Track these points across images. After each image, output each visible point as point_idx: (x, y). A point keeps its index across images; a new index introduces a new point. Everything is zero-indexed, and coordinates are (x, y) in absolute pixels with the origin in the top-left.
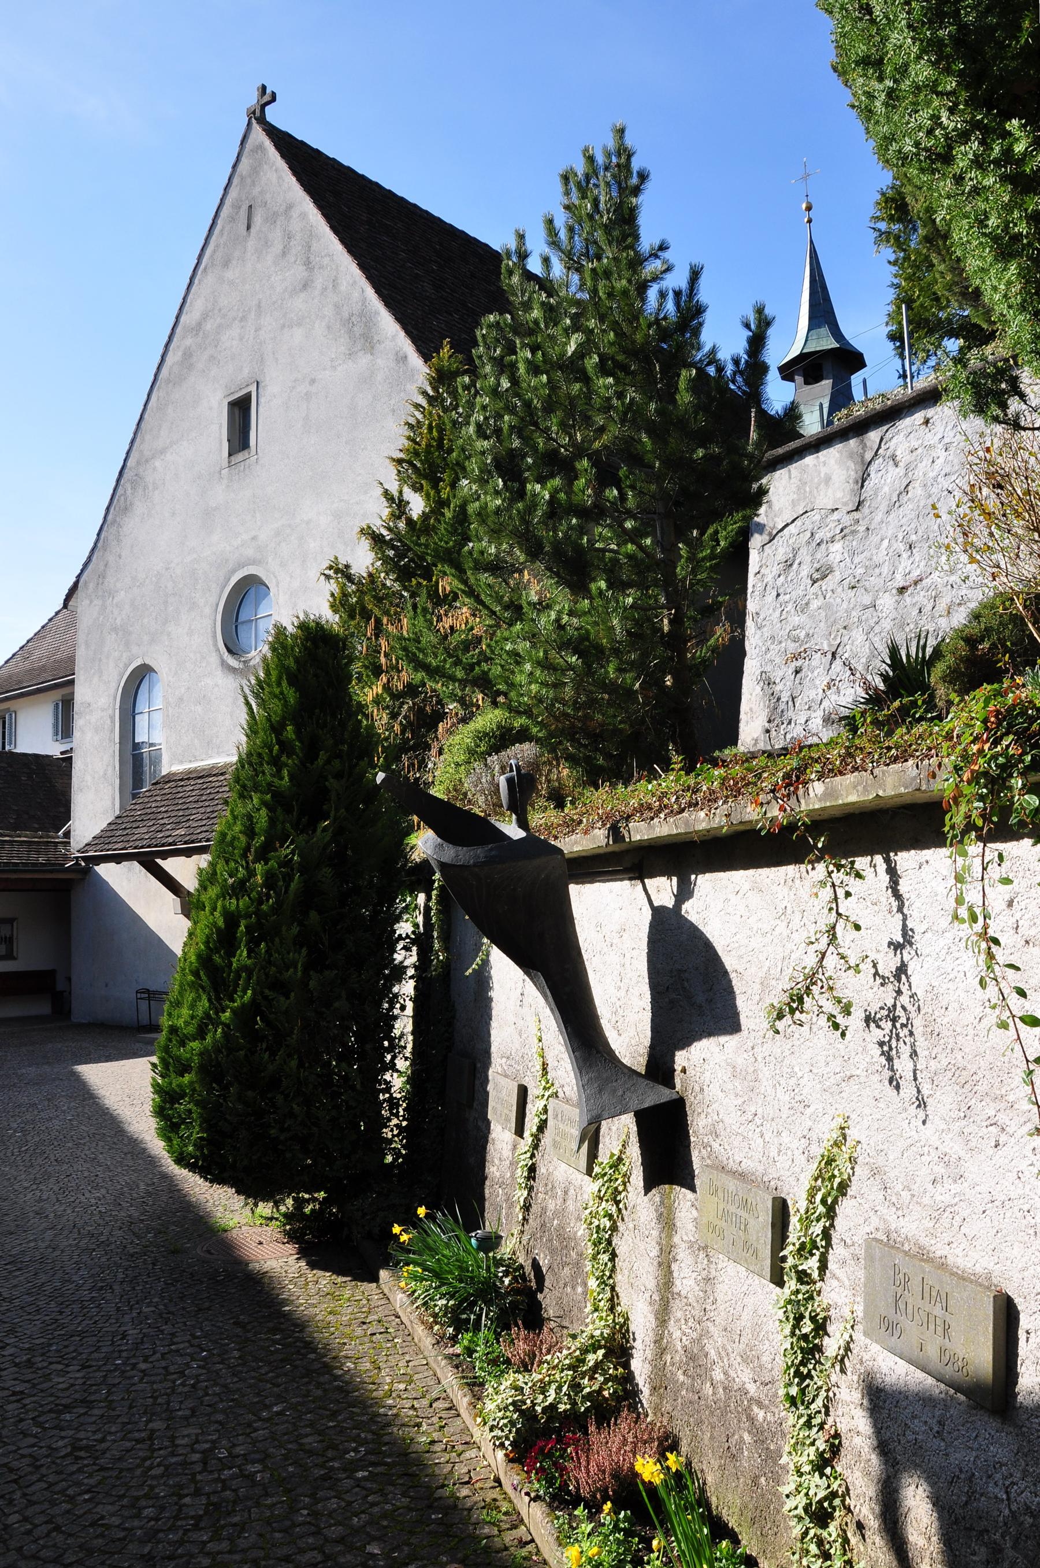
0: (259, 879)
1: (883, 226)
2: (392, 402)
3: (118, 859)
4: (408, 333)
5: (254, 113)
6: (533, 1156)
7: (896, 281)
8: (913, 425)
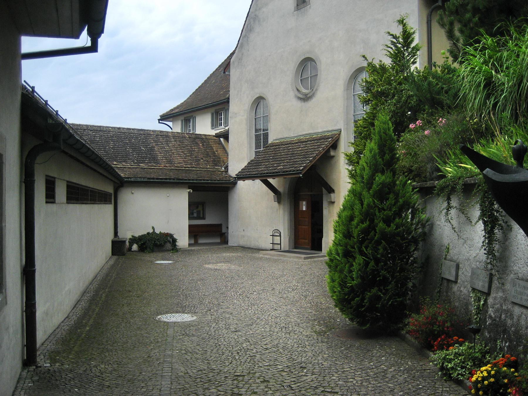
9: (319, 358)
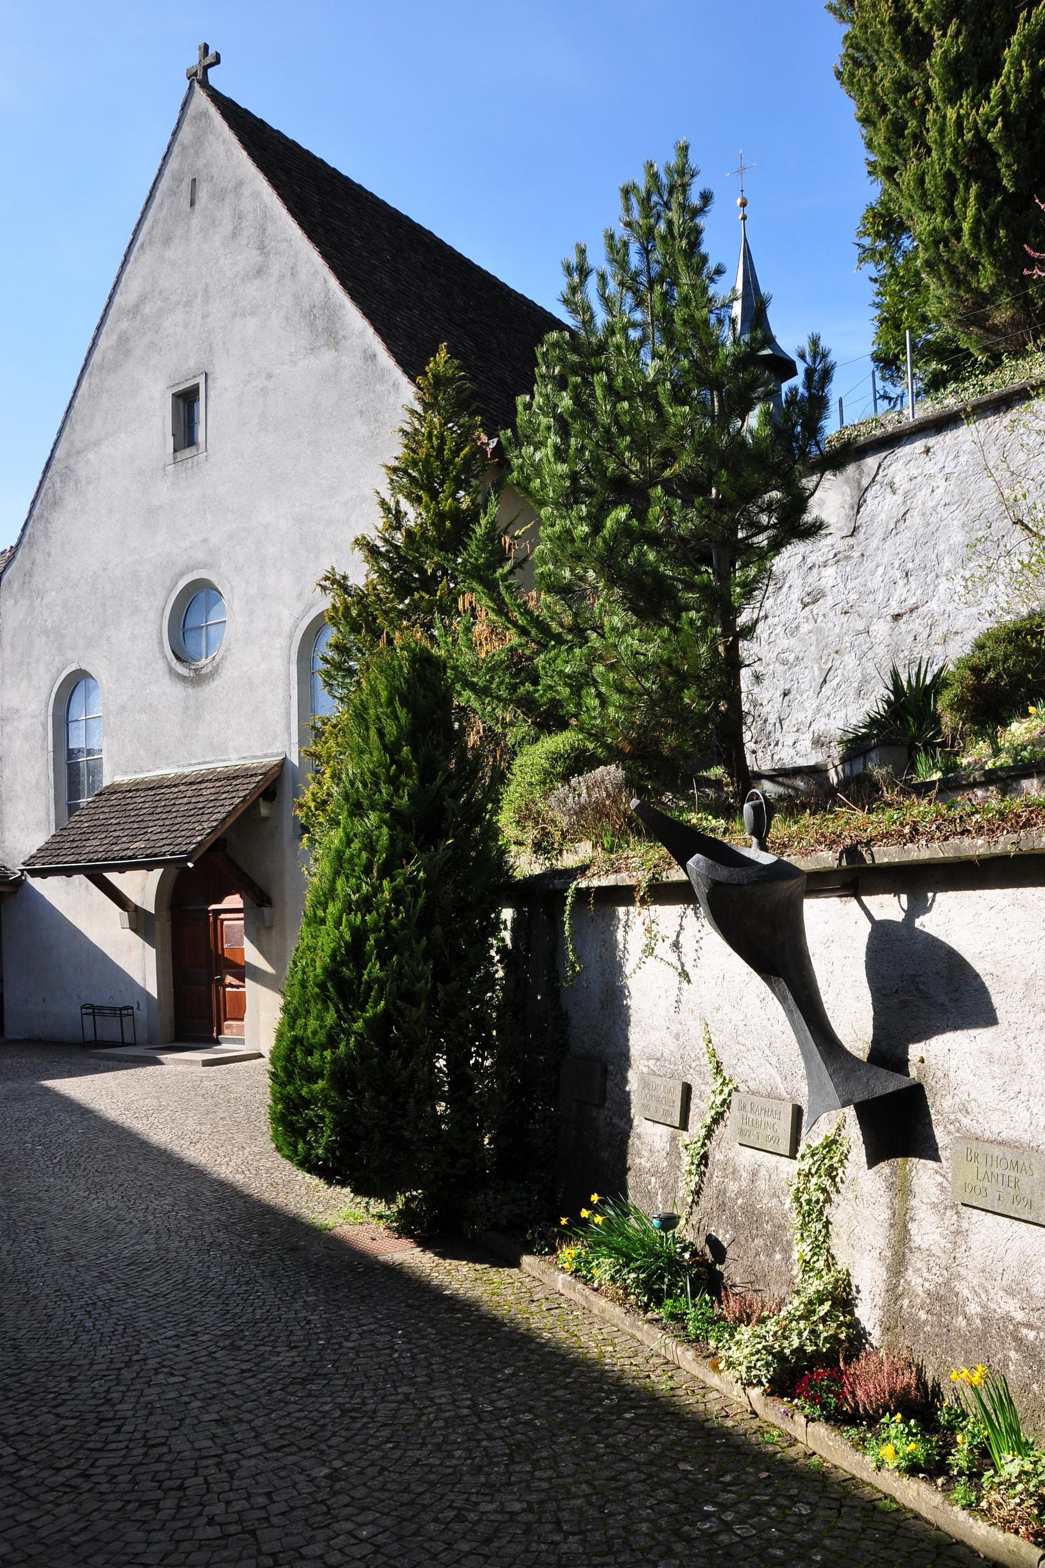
0: (387, 895)
1: (867, 241)
2: (360, 402)
3: (68, 872)
4: (377, 330)
5: (195, 74)
6: (704, 1145)
7: (878, 300)
8: (913, 453)
9: (298, 1306)
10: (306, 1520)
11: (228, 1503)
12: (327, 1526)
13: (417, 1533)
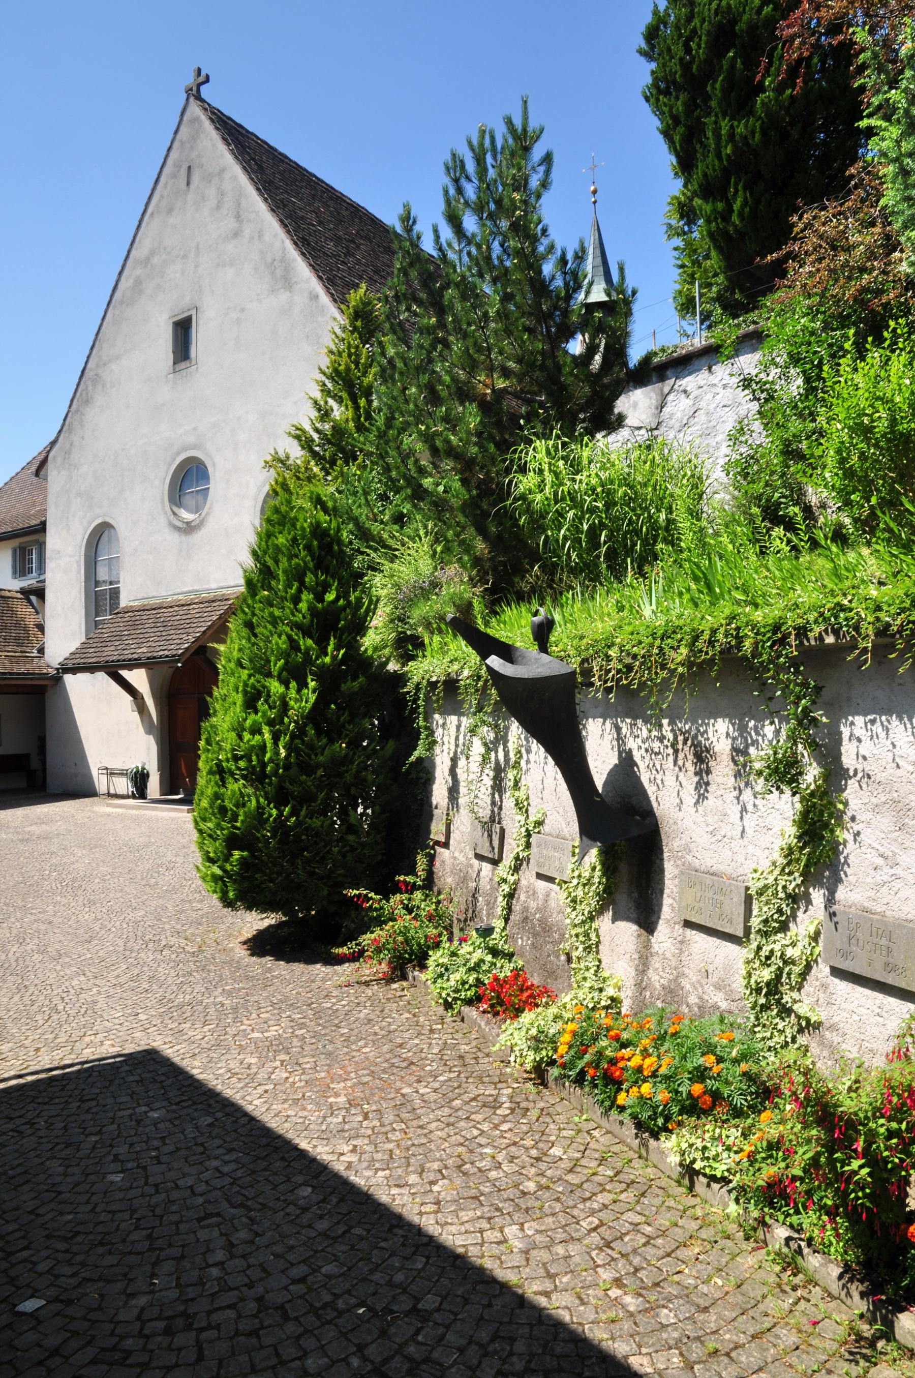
3: (91, 669)
5: (191, 89)
10: (186, 1159)
11: (131, 1145)
12: (201, 1163)
13: (265, 1170)
